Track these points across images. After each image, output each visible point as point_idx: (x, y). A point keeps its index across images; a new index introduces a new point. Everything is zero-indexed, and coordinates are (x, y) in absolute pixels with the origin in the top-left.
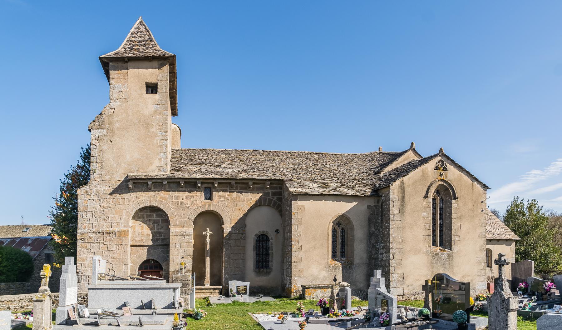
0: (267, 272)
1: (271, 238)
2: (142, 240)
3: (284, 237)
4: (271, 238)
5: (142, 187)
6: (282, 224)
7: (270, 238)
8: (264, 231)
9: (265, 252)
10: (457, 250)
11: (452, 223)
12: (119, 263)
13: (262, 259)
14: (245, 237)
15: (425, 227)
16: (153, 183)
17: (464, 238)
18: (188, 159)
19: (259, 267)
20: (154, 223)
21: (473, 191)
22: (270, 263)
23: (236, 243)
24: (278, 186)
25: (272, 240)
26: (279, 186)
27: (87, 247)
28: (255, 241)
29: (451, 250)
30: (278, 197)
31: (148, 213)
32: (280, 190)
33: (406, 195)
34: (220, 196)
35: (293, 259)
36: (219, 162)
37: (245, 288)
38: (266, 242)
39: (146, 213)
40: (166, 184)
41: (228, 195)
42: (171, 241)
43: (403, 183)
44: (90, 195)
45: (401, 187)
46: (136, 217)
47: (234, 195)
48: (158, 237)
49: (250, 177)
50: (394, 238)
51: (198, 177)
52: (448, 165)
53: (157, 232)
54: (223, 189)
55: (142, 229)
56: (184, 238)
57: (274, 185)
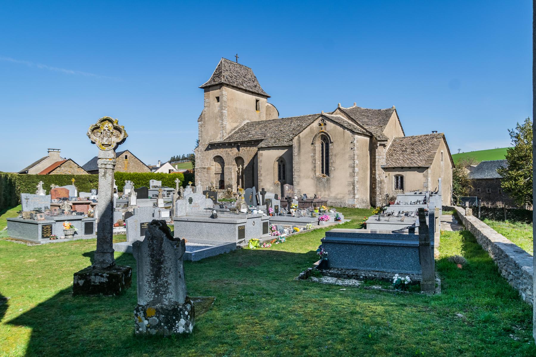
15: (312, 162)
17: (337, 169)
21: (344, 136)
34: (243, 149)
43: (299, 137)
50: (295, 169)
52: (327, 121)
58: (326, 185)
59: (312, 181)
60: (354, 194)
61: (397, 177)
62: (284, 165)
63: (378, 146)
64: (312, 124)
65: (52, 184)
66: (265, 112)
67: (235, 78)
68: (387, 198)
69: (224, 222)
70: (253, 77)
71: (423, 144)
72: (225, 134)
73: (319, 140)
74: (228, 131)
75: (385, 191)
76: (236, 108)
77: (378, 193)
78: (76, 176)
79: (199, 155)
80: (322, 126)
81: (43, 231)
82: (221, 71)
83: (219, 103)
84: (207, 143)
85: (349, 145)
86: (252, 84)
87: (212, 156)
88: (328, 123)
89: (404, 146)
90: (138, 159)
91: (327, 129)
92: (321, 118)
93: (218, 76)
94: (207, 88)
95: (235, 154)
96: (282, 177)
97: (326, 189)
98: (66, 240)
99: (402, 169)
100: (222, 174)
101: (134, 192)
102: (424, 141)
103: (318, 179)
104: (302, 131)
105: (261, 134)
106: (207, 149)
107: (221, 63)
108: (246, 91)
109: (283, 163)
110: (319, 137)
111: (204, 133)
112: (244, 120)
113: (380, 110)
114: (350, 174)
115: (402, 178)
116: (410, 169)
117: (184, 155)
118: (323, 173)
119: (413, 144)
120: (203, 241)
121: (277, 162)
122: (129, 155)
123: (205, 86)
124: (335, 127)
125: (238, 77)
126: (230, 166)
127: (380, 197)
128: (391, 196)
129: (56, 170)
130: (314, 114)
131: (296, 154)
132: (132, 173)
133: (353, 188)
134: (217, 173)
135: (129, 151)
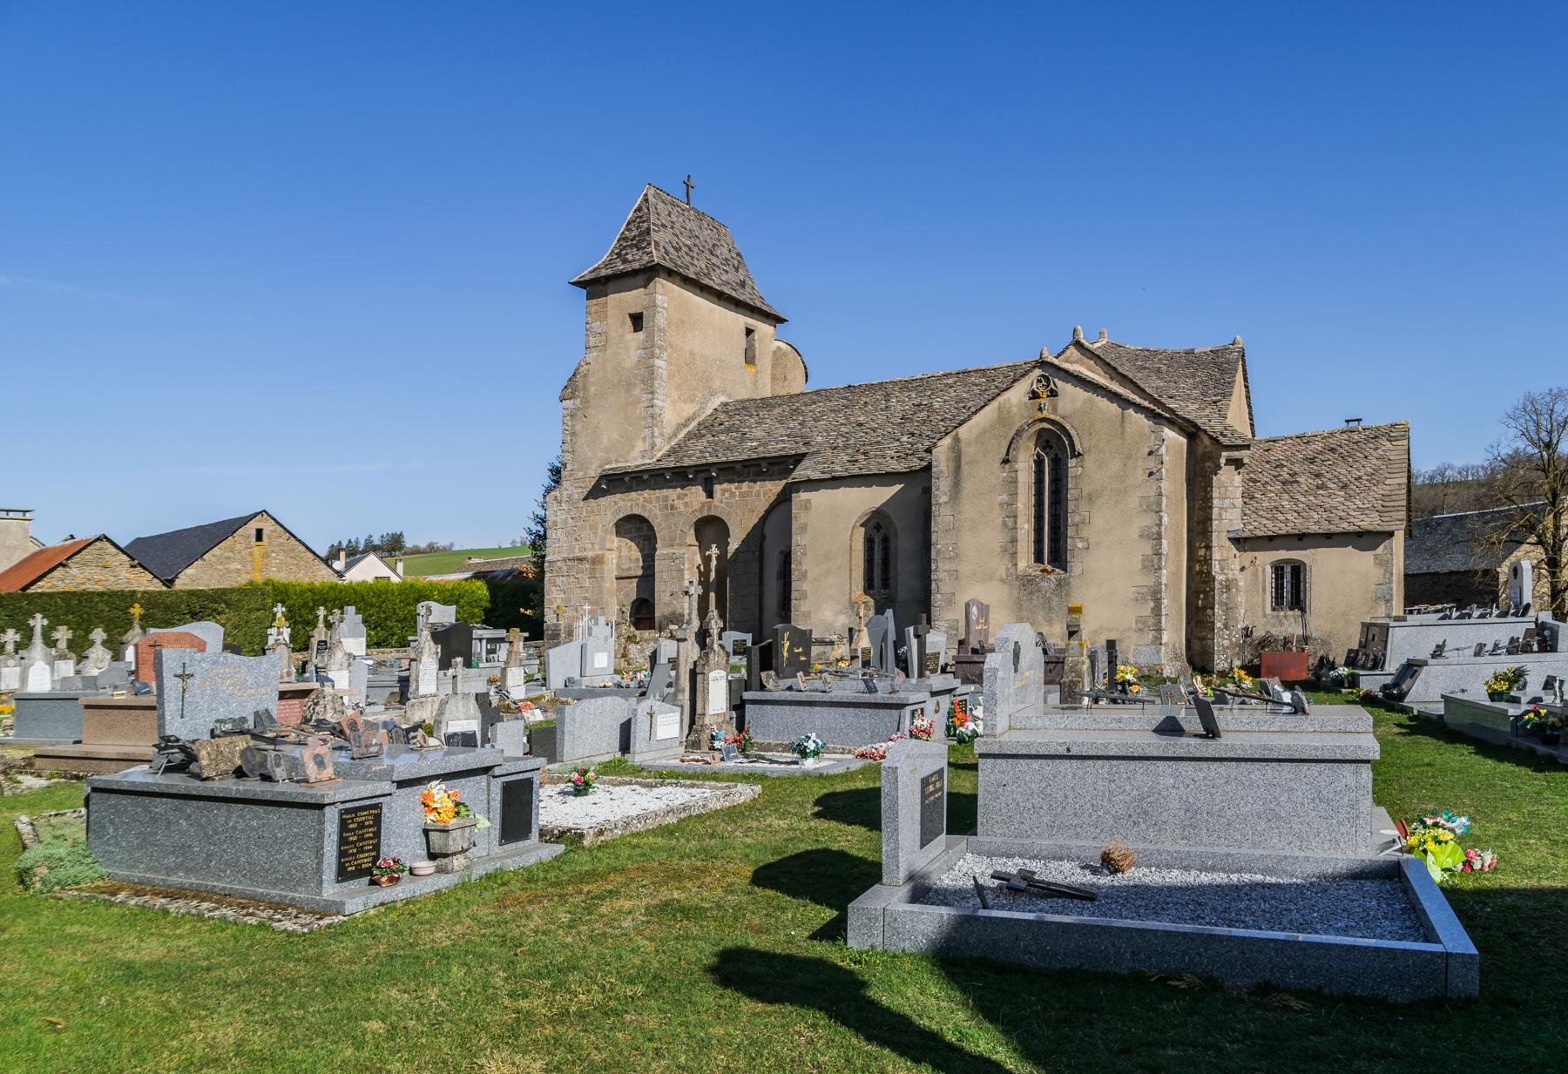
2: (630, 568)
10: (1079, 570)
11: (1070, 511)
15: (1004, 523)
17: (1098, 544)
20: (644, 540)
21: (1123, 432)
29: (1065, 570)
33: (963, 463)
34: (724, 491)
41: (736, 488)
43: (957, 440)
44: (560, 503)
45: (954, 448)
47: (745, 486)
50: (938, 551)
55: (630, 551)
58: (1055, 601)
59: (1005, 588)
60: (1159, 630)
61: (1278, 569)
62: (886, 540)
63: (1222, 465)
64: (1006, 395)
65: (61, 628)
66: (769, 372)
67: (687, 254)
68: (1244, 642)
69: (1297, 756)
70: (734, 256)
71: (1350, 460)
72: (658, 441)
73: (1028, 448)
74: (668, 431)
75: (1241, 618)
76: (692, 353)
77: (1218, 625)
78: (142, 597)
79: (561, 517)
80: (1042, 401)
81: (343, 841)
82: (649, 229)
83: (641, 335)
84: (594, 472)
85: (1140, 462)
86: (731, 277)
87: (609, 517)
88: (1065, 388)
89: (1283, 466)
90: (299, 541)
91: (1061, 410)
92: (1038, 372)
93: (635, 245)
94: (596, 286)
95: (696, 506)
96: (877, 581)
97: (1053, 616)
98: (444, 881)
99: (1302, 539)
100: (647, 578)
101: (432, 643)
102: (1347, 448)
103: (1026, 582)
104: (969, 418)
105: (788, 436)
106: (595, 493)
107: (646, 200)
108: (720, 297)
109: (883, 531)
110: (1029, 438)
111: (581, 440)
112: (713, 394)
113: (1192, 352)
114: (1143, 561)
115: (1298, 570)
116: (1329, 539)
117: (371, 536)
118: (1039, 558)
119: (1312, 461)
120: (1214, 855)
121: (863, 529)
122: (268, 527)
123: (592, 276)
124: (1091, 400)
125: (696, 249)
126: (677, 551)
127: (1224, 639)
128: (1259, 633)
129: (49, 576)
130: (962, 368)
131: (944, 499)
132: (317, 584)
133: (1153, 609)
134: (624, 575)
135: (269, 516)
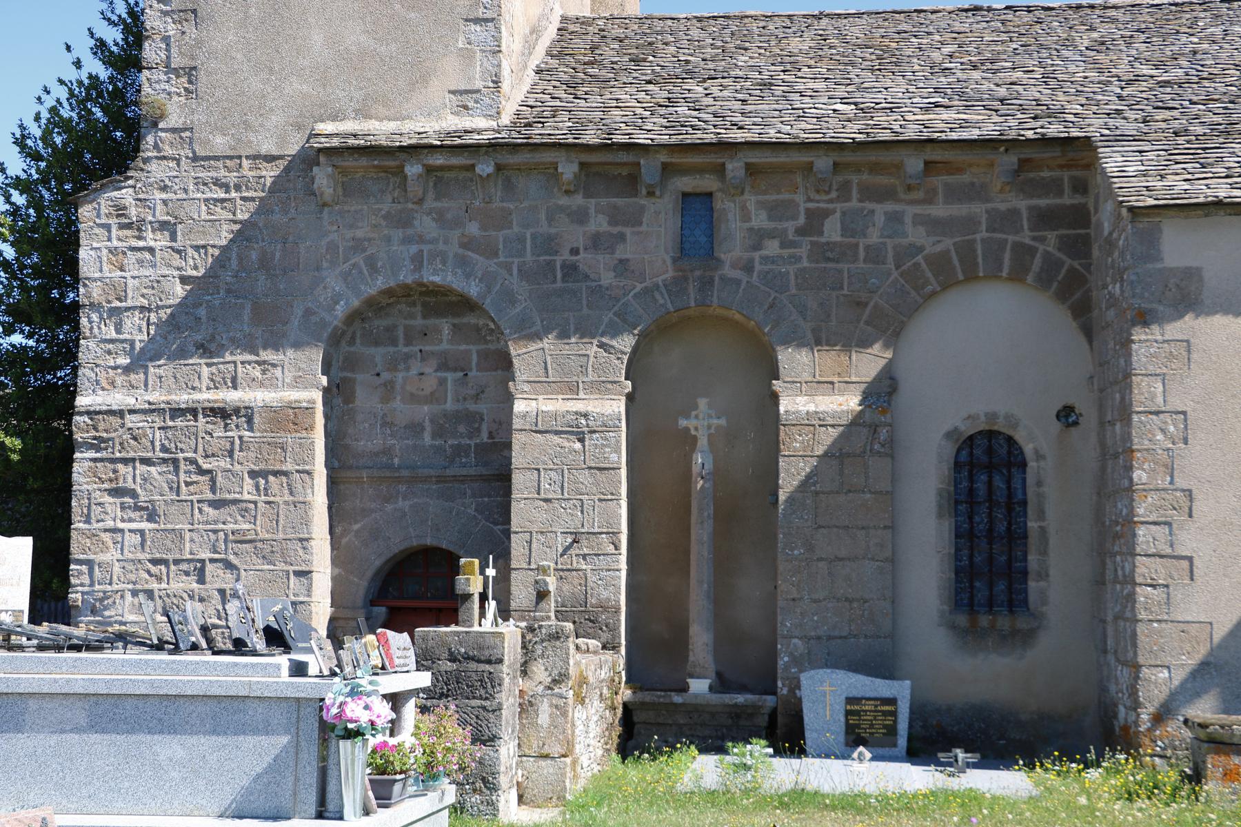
0: (1014, 633)
1: (1036, 451)
3: (1102, 444)
4: (1036, 451)
5: (382, 192)
6: (1092, 377)
7: (1028, 449)
8: (992, 417)
9: (1001, 527)
12: (270, 563)
13: (991, 560)
14: (891, 442)
16: (429, 170)
18: (626, 58)
19: (971, 605)
22: (1032, 584)
23: (841, 474)
24: (1066, 175)
25: (1042, 463)
26: (1072, 178)
27: (116, 479)
28: (946, 468)
30: (1068, 236)
31: (412, 322)
32: (1078, 200)
35: (1144, 568)
36: (773, 68)
37: (885, 713)
38: (1009, 471)
39: (407, 322)
40: (488, 175)
42: (518, 458)
46: (358, 341)
48: (461, 436)
49: (911, 133)
51: (642, 138)
53: (457, 411)
54: (774, 197)
56: (578, 446)
57: (1046, 174)
